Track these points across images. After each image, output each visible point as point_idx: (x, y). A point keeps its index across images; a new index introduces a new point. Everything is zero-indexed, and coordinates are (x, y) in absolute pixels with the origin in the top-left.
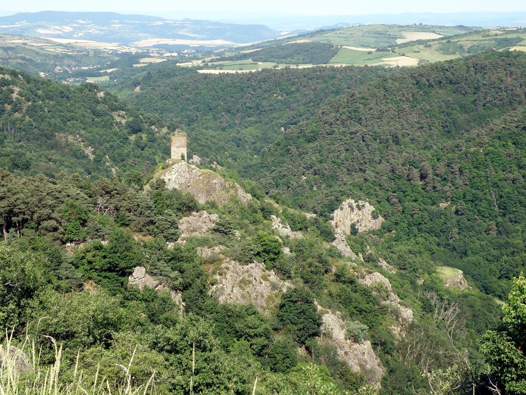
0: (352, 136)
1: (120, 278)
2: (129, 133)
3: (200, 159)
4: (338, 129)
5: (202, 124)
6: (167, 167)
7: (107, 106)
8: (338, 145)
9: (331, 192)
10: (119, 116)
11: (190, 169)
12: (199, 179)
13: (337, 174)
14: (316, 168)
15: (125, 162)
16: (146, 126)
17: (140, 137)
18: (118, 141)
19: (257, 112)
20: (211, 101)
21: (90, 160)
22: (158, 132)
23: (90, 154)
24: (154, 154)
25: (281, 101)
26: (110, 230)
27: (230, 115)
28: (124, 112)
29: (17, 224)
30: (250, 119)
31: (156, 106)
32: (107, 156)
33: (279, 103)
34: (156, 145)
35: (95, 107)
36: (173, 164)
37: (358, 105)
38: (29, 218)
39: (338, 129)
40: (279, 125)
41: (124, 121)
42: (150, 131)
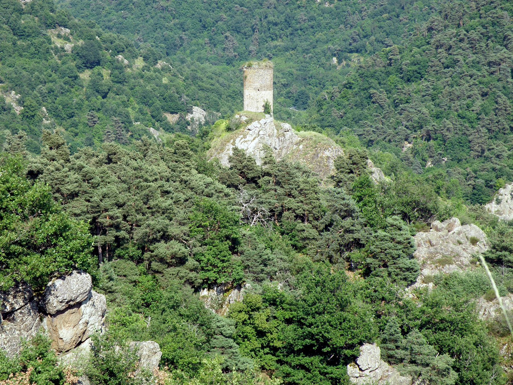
0: (493, 69)
1: (330, 369)
2: (79, 68)
3: (205, 113)
4: (465, 57)
5: (192, 52)
6: (238, 127)
7: (36, 19)
8: (467, 85)
9: (475, 172)
10: (59, 36)
11: (281, 132)
12: (299, 151)
13: (470, 138)
14: (430, 128)
15: (76, 119)
16: (107, 55)
17: (99, 74)
18: (61, 82)
19: (289, 31)
20: (205, 12)
21: (14, 114)
22: (130, 66)
23: (14, 105)
24: (125, 104)
25: (330, 12)
26: (285, 261)
27: (239, 37)
28: (68, 31)
29: (100, 250)
30: (275, 43)
31: (109, 21)
32: (44, 109)
33: (325, 15)
34: (126, 88)
35: (15, 21)
36: (248, 122)
37: (500, 13)
38: (127, 236)
39: (465, 57)
40: (329, 54)
41: (68, 46)
42: (116, 64)
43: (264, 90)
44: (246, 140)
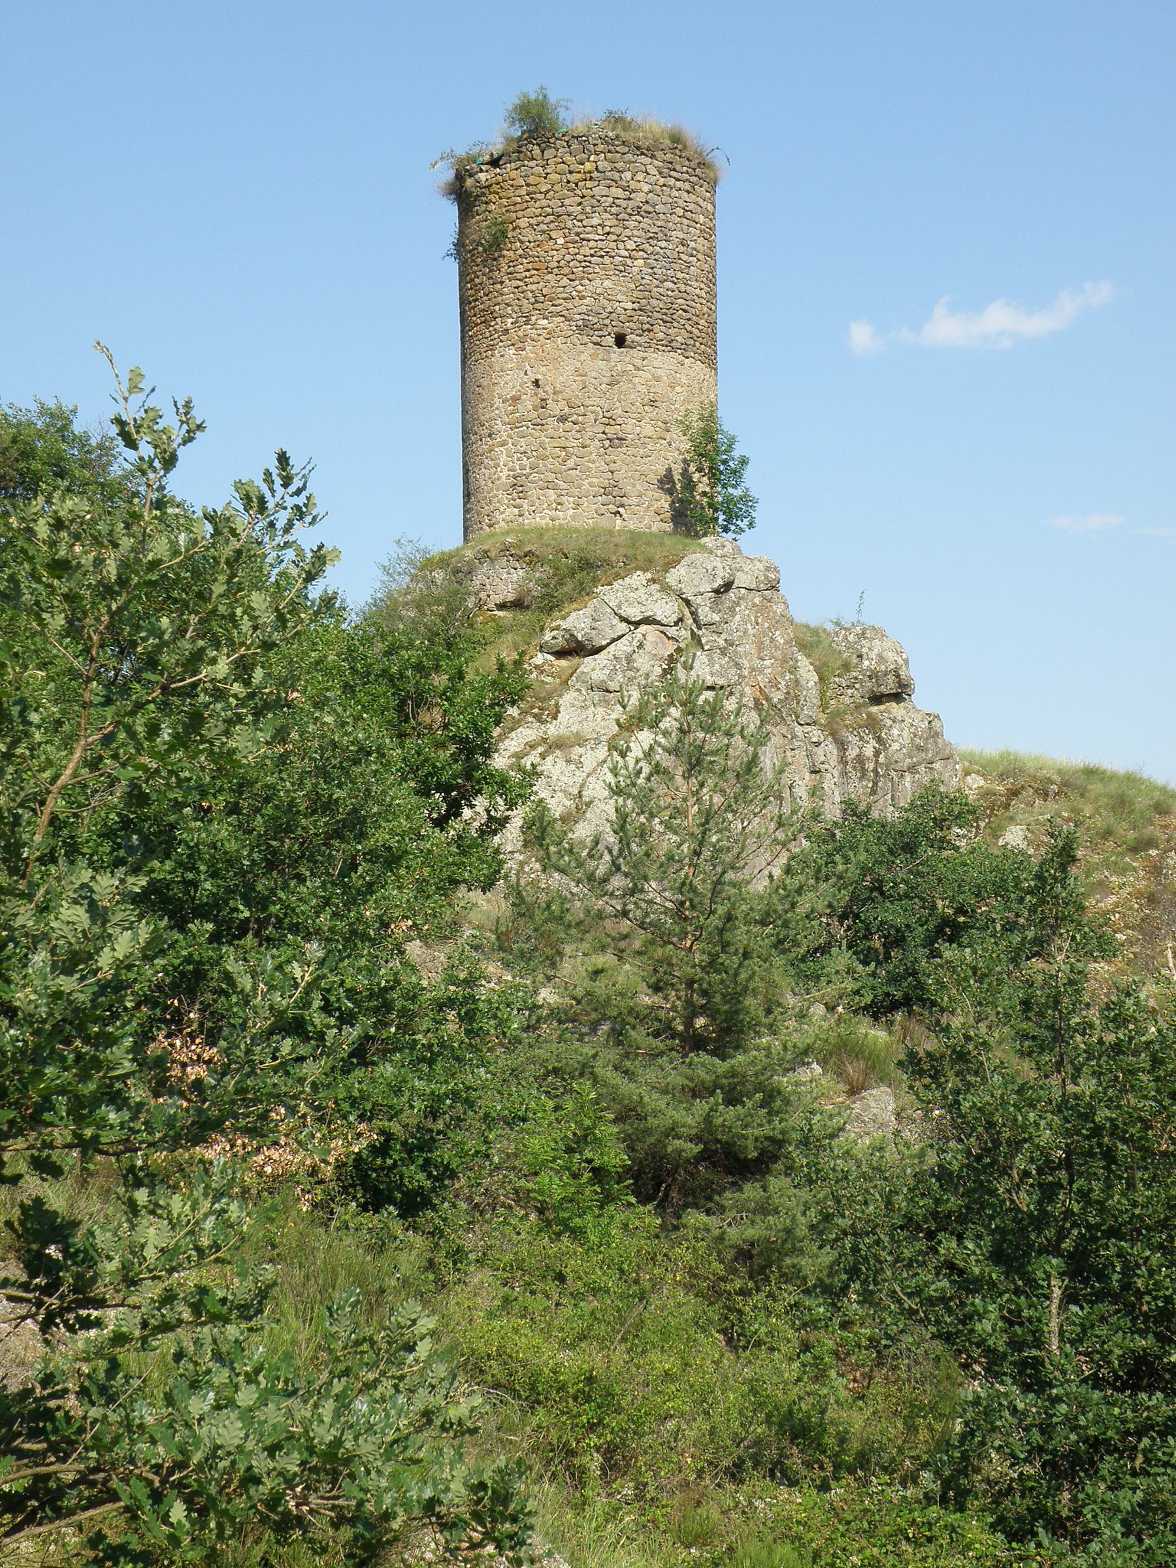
43: (670, 345)
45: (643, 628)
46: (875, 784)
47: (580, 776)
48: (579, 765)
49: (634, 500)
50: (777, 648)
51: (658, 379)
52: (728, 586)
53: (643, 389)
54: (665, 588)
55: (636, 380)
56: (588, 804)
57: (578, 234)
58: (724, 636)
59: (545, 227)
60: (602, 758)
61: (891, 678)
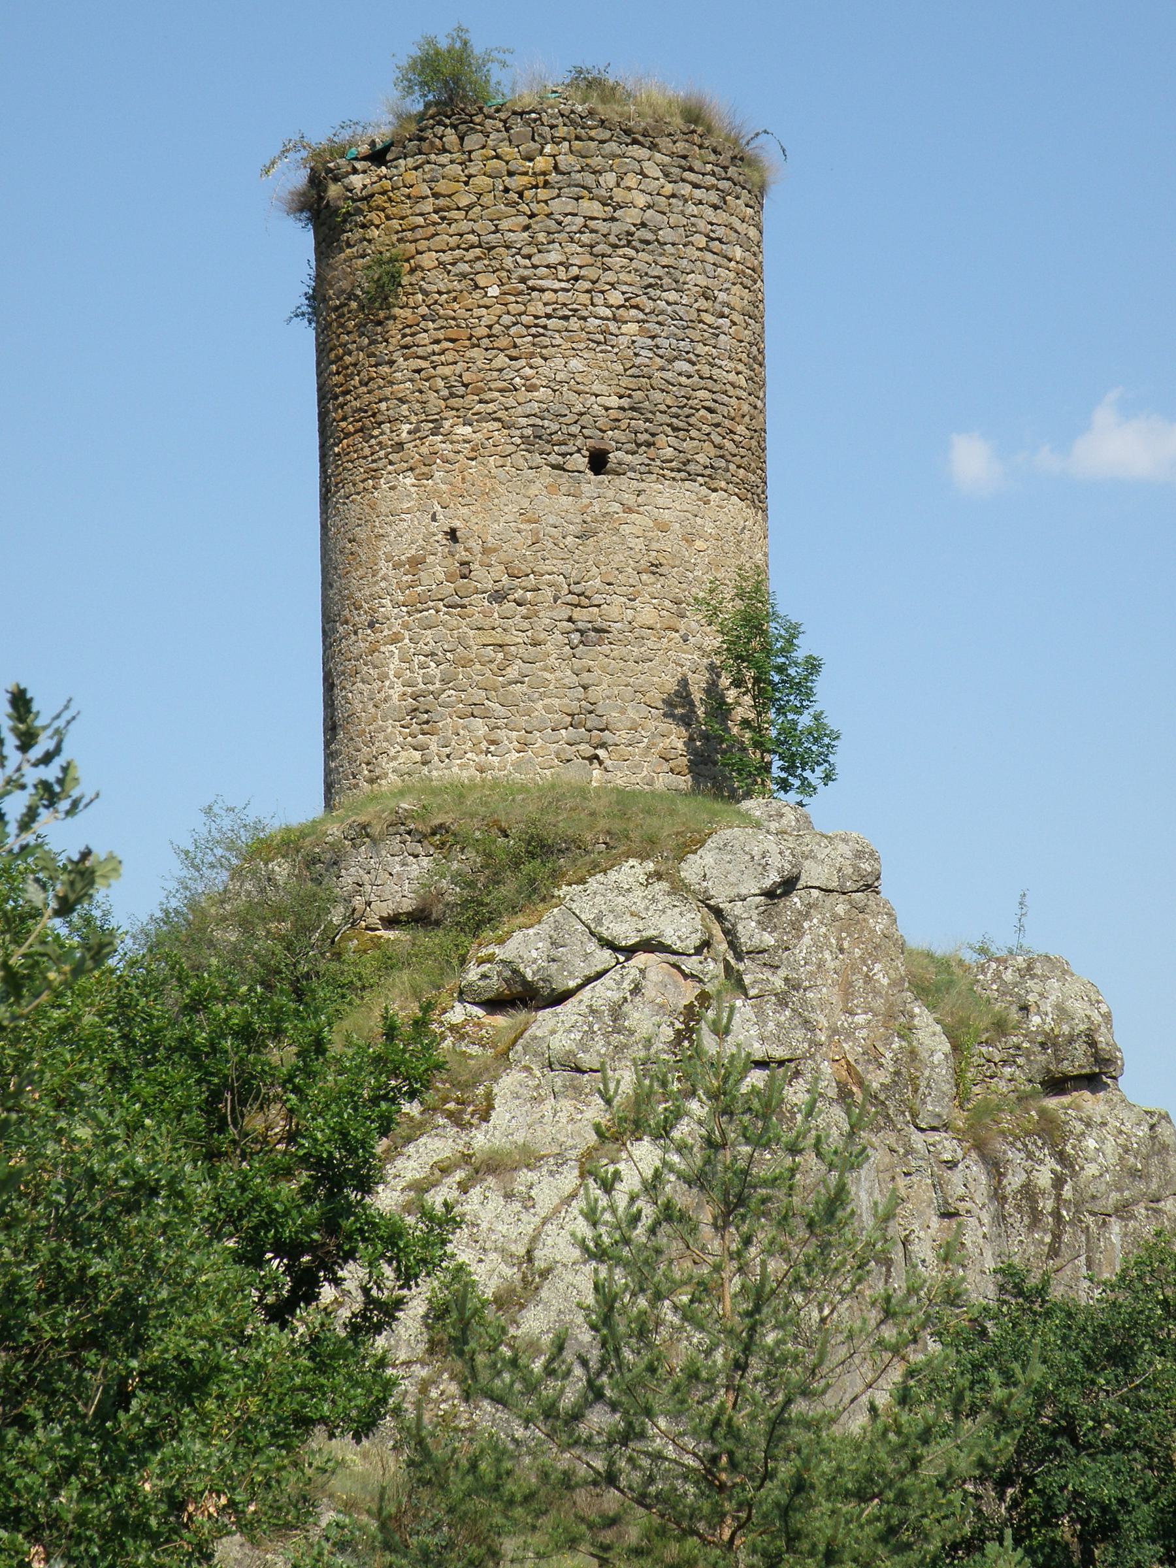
43: (684, 469)
44: (481, 1140)
45: (641, 959)
46: (1057, 1237)
47: (529, 1223)
48: (528, 1203)
49: (622, 736)
50: (876, 993)
51: (664, 528)
52: (789, 884)
53: (639, 544)
54: (679, 889)
55: (626, 529)
56: (544, 1274)
57: (523, 280)
58: (782, 973)
59: (465, 268)
60: (568, 1189)
61: (1080, 1048)
